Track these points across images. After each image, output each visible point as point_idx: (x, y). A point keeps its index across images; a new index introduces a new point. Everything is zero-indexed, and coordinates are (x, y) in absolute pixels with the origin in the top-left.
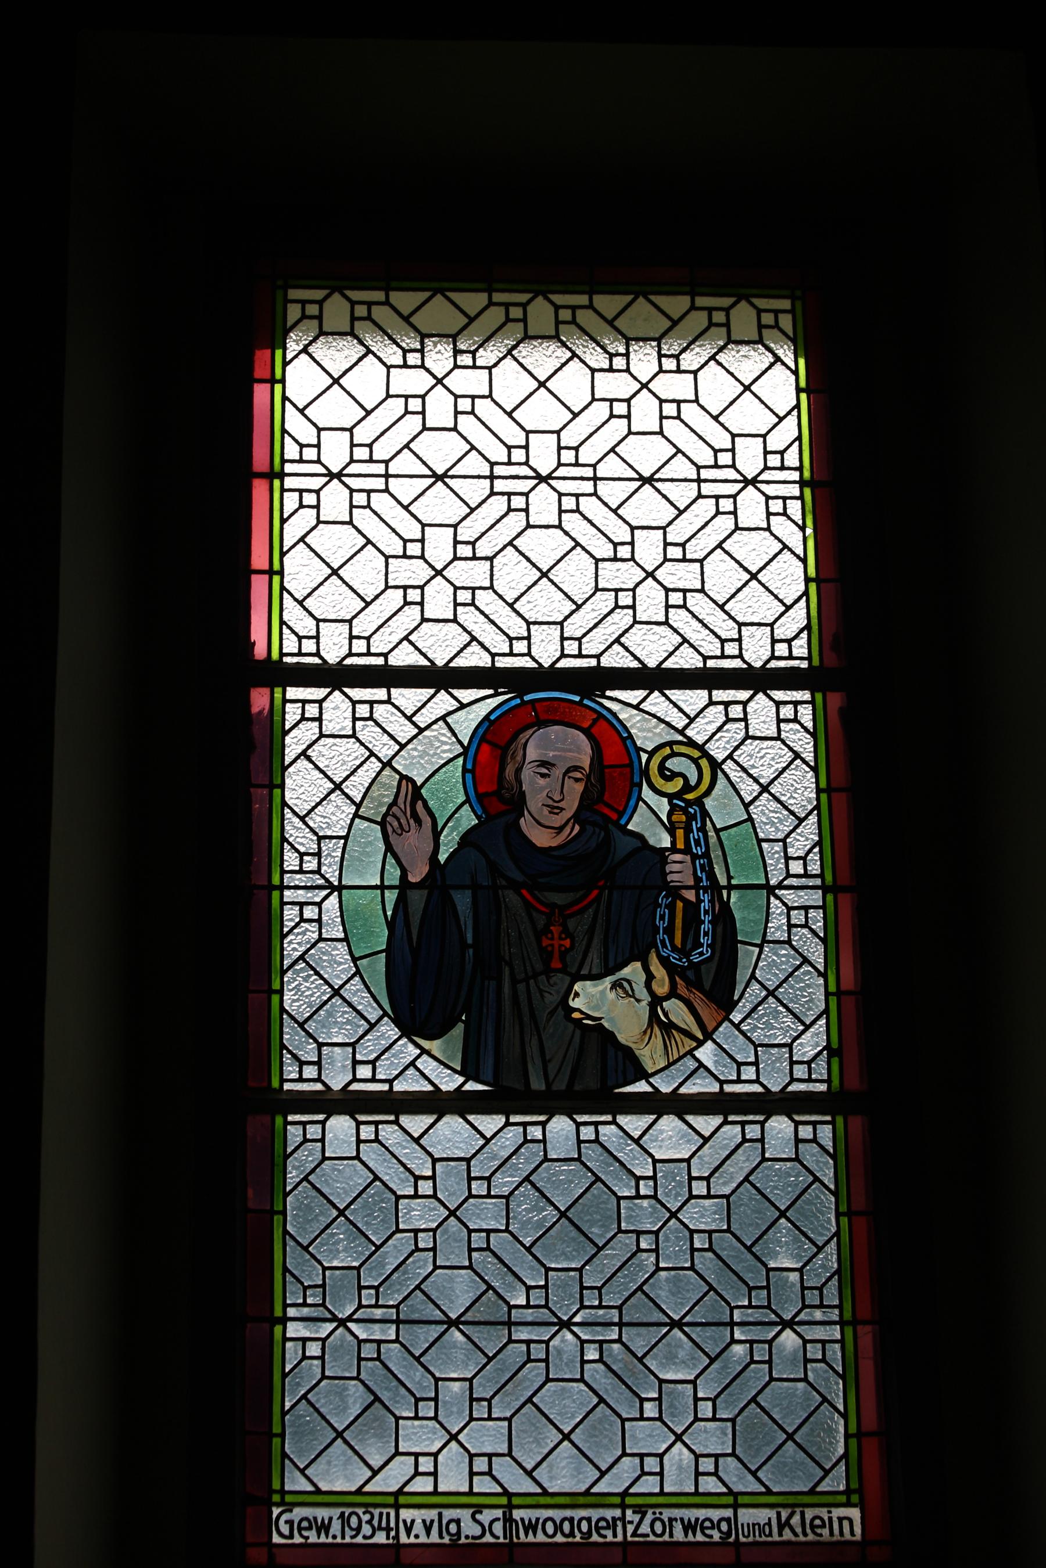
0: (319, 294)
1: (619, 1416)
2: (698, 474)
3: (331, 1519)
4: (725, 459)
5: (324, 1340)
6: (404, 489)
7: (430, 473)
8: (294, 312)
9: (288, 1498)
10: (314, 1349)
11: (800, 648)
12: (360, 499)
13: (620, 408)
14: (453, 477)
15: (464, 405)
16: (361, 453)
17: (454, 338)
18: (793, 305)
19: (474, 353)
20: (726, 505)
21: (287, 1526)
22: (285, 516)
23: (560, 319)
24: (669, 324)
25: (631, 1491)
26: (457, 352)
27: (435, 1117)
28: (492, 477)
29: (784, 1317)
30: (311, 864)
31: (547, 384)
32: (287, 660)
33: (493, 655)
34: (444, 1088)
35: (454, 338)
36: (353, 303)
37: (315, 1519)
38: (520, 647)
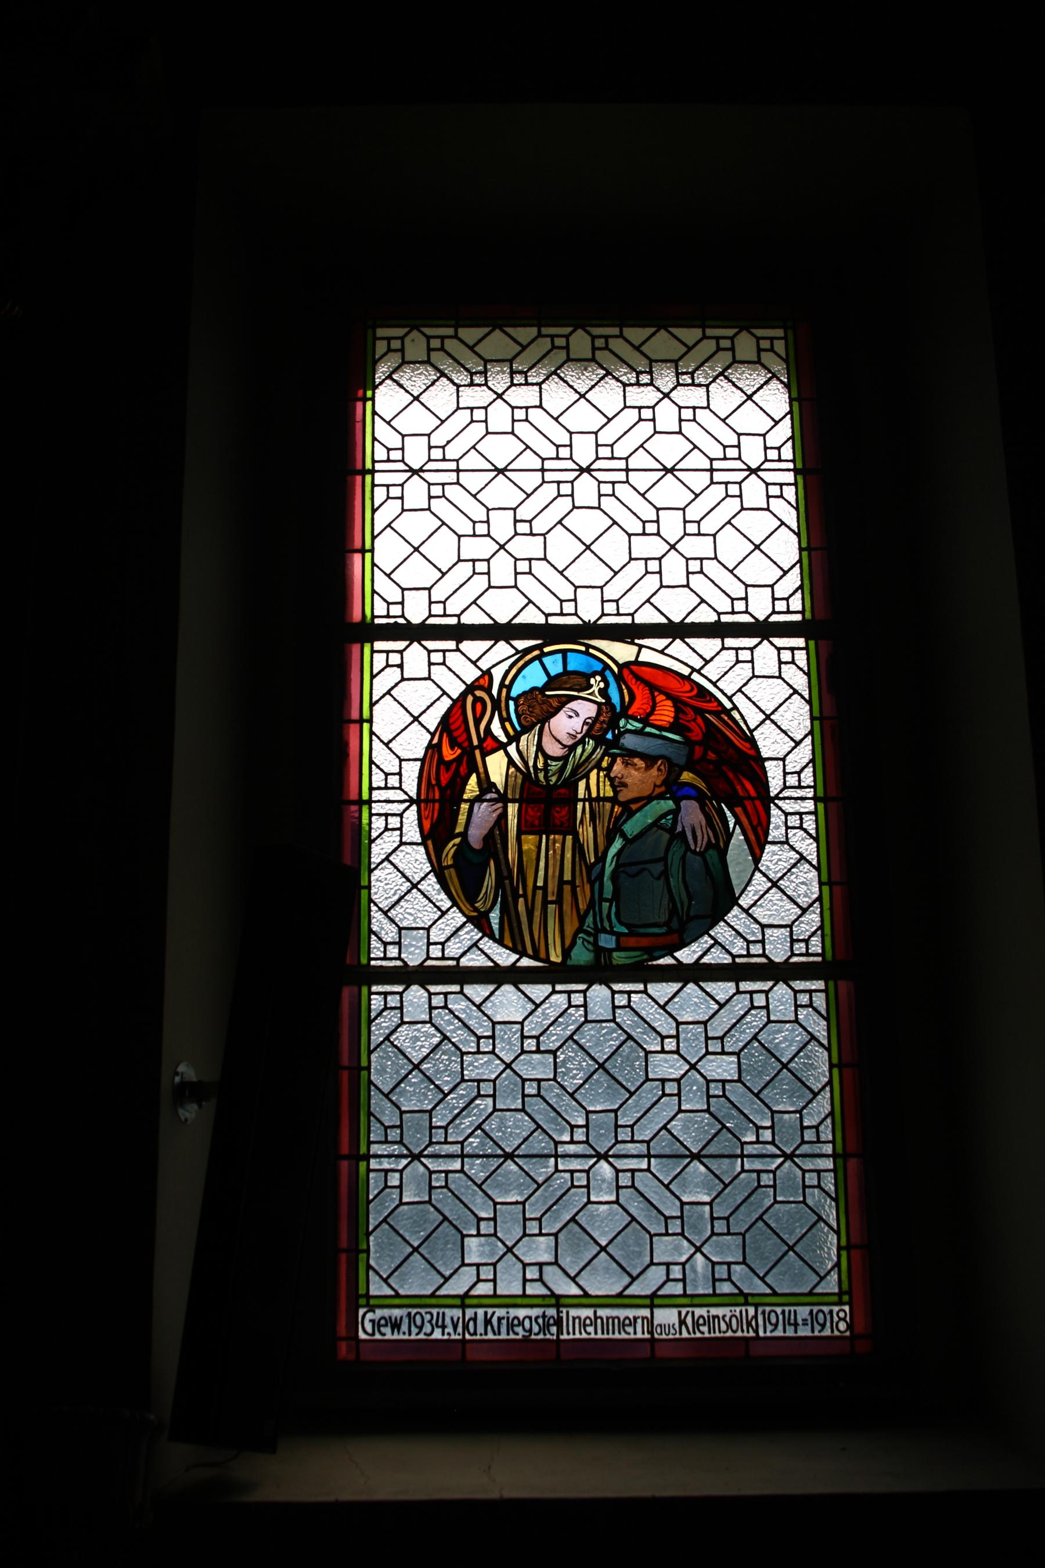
0: (400, 332)
1: (648, 1232)
2: (711, 465)
3: (401, 1318)
4: (564, 452)
5: (774, 1172)
6: (641, 480)
7: (662, 467)
8: (381, 347)
9: (372, 1302)
10: (766, 1179)
11: (796, 604)
12: (606, 489)
13: (647, 414)
14: (424, 471)
15: (687, 414)
16: (437, 454)
17: (511, 361)
18: (785, 333)
19: (692, 374)
20: (566, 489)
21: (371, 1324)
22: (376, 505)
23: (432, 346)
24: (684, 349)
25: (660, 1293)
26: (512, 373)
27: (495, 986)
28: (712, 470)
29: (507, 1150)
30: (393, 781)
31: (412, 398)
32: (377, 621)
33: (719, 614)
34: (411, 964)
35: (676, 362)
36: (429, 338)
37: (390, 1318)
38: (740, 606)
